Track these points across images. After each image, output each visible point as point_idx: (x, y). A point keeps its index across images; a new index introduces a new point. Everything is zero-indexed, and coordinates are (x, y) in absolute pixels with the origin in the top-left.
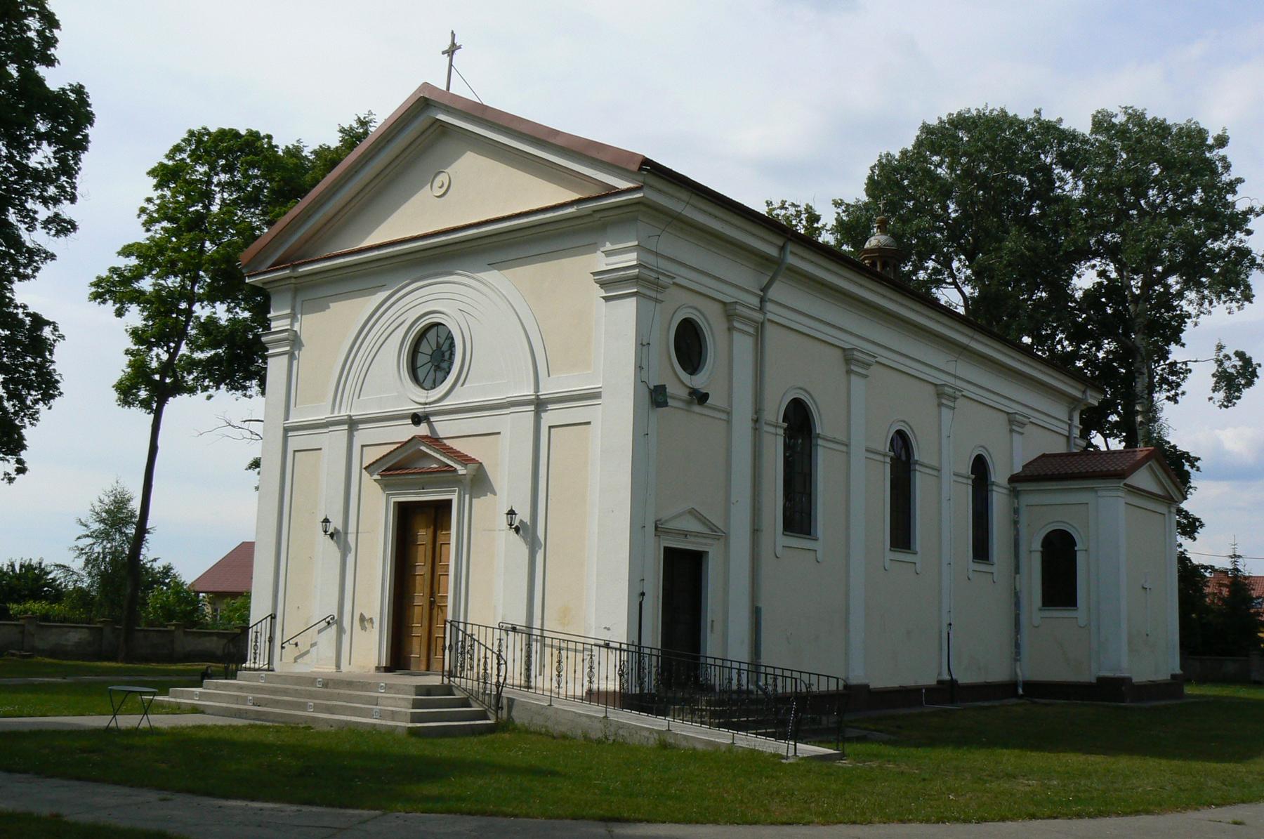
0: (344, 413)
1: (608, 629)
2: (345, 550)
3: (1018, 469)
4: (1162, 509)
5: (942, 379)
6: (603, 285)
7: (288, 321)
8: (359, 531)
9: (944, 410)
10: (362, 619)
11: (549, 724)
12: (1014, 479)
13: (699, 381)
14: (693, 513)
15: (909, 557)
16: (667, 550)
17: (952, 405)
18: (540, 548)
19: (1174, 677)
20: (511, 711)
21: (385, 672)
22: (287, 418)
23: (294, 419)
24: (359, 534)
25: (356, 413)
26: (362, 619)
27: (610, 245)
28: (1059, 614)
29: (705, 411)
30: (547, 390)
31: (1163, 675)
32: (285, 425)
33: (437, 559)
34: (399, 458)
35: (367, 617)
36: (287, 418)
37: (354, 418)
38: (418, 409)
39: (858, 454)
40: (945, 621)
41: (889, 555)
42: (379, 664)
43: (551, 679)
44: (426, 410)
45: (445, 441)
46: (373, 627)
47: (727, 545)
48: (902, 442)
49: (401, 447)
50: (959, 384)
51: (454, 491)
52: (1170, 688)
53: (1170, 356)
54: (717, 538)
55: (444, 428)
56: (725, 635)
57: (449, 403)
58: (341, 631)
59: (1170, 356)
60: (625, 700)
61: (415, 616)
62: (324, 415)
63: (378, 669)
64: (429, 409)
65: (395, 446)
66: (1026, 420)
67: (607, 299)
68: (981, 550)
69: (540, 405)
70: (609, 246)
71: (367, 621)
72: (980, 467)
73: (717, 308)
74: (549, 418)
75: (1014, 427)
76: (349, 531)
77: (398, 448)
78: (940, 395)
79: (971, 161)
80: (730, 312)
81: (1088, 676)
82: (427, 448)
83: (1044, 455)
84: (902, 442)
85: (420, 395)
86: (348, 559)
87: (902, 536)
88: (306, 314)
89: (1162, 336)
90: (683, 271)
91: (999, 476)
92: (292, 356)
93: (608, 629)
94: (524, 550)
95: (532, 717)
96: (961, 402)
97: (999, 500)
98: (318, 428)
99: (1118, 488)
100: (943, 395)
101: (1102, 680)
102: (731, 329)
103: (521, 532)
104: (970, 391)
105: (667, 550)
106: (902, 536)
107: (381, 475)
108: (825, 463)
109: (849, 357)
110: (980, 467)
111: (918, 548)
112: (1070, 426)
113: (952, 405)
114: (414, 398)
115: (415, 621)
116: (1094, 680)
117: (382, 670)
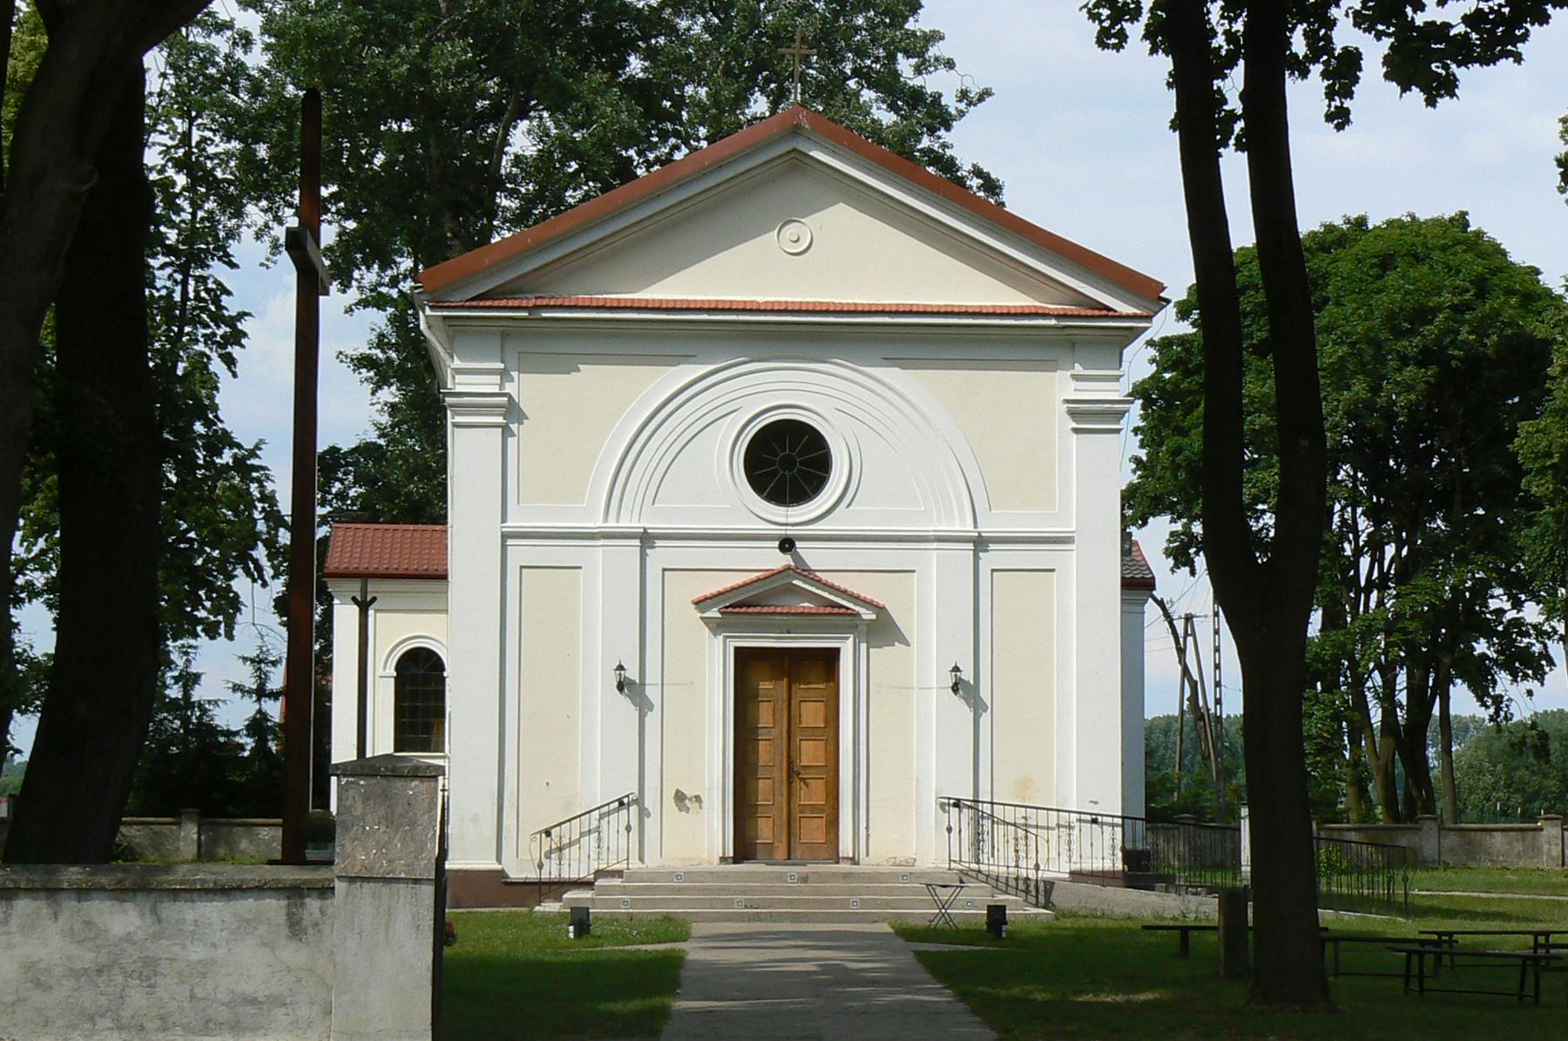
1: (1096, 803)
2: (643, 706)
6: (1073, 414)
7: (497, 379)
8: (665, 682)
10: (680, 797)
11: (1105, 907)
18: (985, 711)
20: (1050, 896)
21: (735, 863)
22: (504, 520)
23: (513, 523)
24: (1519, 833)
25: (655, 525)
26: (680, 797)
27: (1081, 368)
30: (988, 528)
32: (504, 530)
33: (794, 721)
34: (752, 593)
35: (689, 793)
36: (504, 520)
37: (649, 531)
42: (724, 853)
43: (608, 848)
44: (788, 532)
45: (817, 574)
46: (701, 808)
49: (766, 578)
51: (848, 638)
53: (1536, 25)
58: (643, 813)
59: (1536, 25)
61: (760, 791)
63: (723, 860)
65: (753, 576)
67: (1076, 431)
69: (980, 543)
70: (1078, 369)
71: (690, 799)
74: (989, 560)
76: (647, 682)
77: (758, 580)
82: (805, 582)
86: (646, 719)
88: (524, 373)
92: (506, 431)
93: (1096, 803)
94: (969, 714)
95: (160, 921)
98: (558, 538)
103: (961, 692)
107: (721, 613)
115: (760, 797)
117: (731, 860)
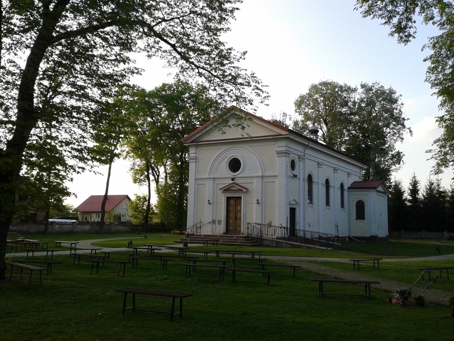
0: (212, 176)
3: (349, 186)
4: (384, 195)
5: (335, 166)
6: (278, 153)
9: (300, 162)
12: (349, 188)
13: (295, 172)
14: (294, 200)
15: (312, 205)
16: (227, 197)
17: (288, 156)
19: (387, 236)
28: (360, 222)
29: (296, 179)
31: (385, 236)
38: (233, 177)
39: (320, 185)
40: (336, 222)
41: (326, 207)
47: (299, 206)
48: (327, 181)
50: (339, 167)
52: (383, 240)
54: (297, 205)
55: (238, 181)
56: (300, 225)
57: (240, 176)
60: (224, 233)
62: (207, 176)
64: (235, 177)
66: (290, 153)
67: (278, 156)
68: (342, 206)
72: (342, 185)
73: (297, 156)
75: (319, 166)
78: (335, 170)
79: (361, 124)
80: (299, 157)
81: (367, 235)
83: (355, 182)
84: (327, 181)
85: (233, 174)
87: (328, 203)
89: (356, 135)
90: (292, 150)
91: (346, 187)
96: (339, 171)
97: (346, 193)
99: (375, 191)
100: (335, 170)
101: (372, 237)
102: (299, 161)
104: (354, 173)
105: (227, 197)
106: (328, 203)
108: (315, 187)
109: (319, 164)
110: (342, 185)
111: (314, 203)
112: (304, 153)
113: (288, 156)
114: (232, 174)
116: (369, 236)
